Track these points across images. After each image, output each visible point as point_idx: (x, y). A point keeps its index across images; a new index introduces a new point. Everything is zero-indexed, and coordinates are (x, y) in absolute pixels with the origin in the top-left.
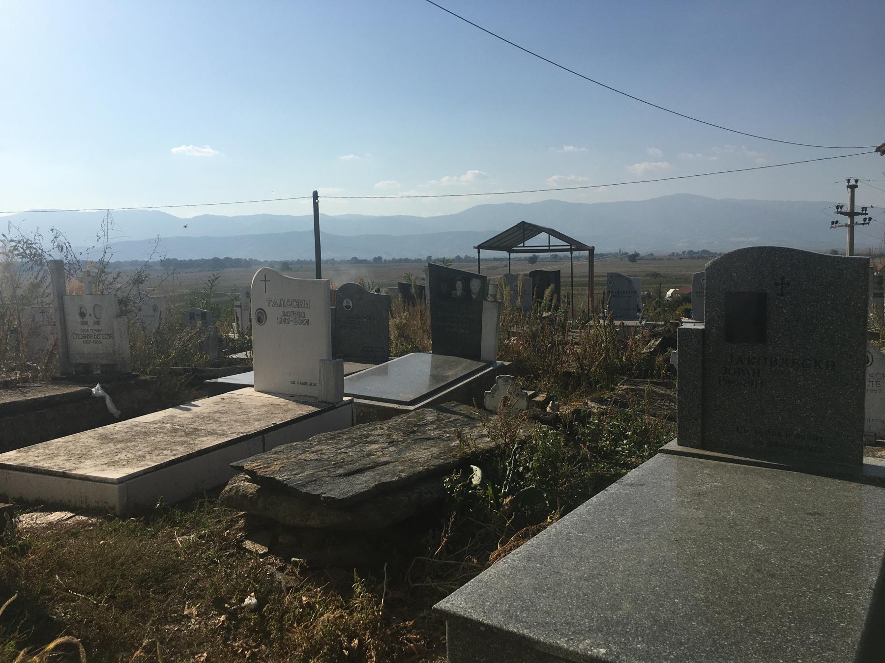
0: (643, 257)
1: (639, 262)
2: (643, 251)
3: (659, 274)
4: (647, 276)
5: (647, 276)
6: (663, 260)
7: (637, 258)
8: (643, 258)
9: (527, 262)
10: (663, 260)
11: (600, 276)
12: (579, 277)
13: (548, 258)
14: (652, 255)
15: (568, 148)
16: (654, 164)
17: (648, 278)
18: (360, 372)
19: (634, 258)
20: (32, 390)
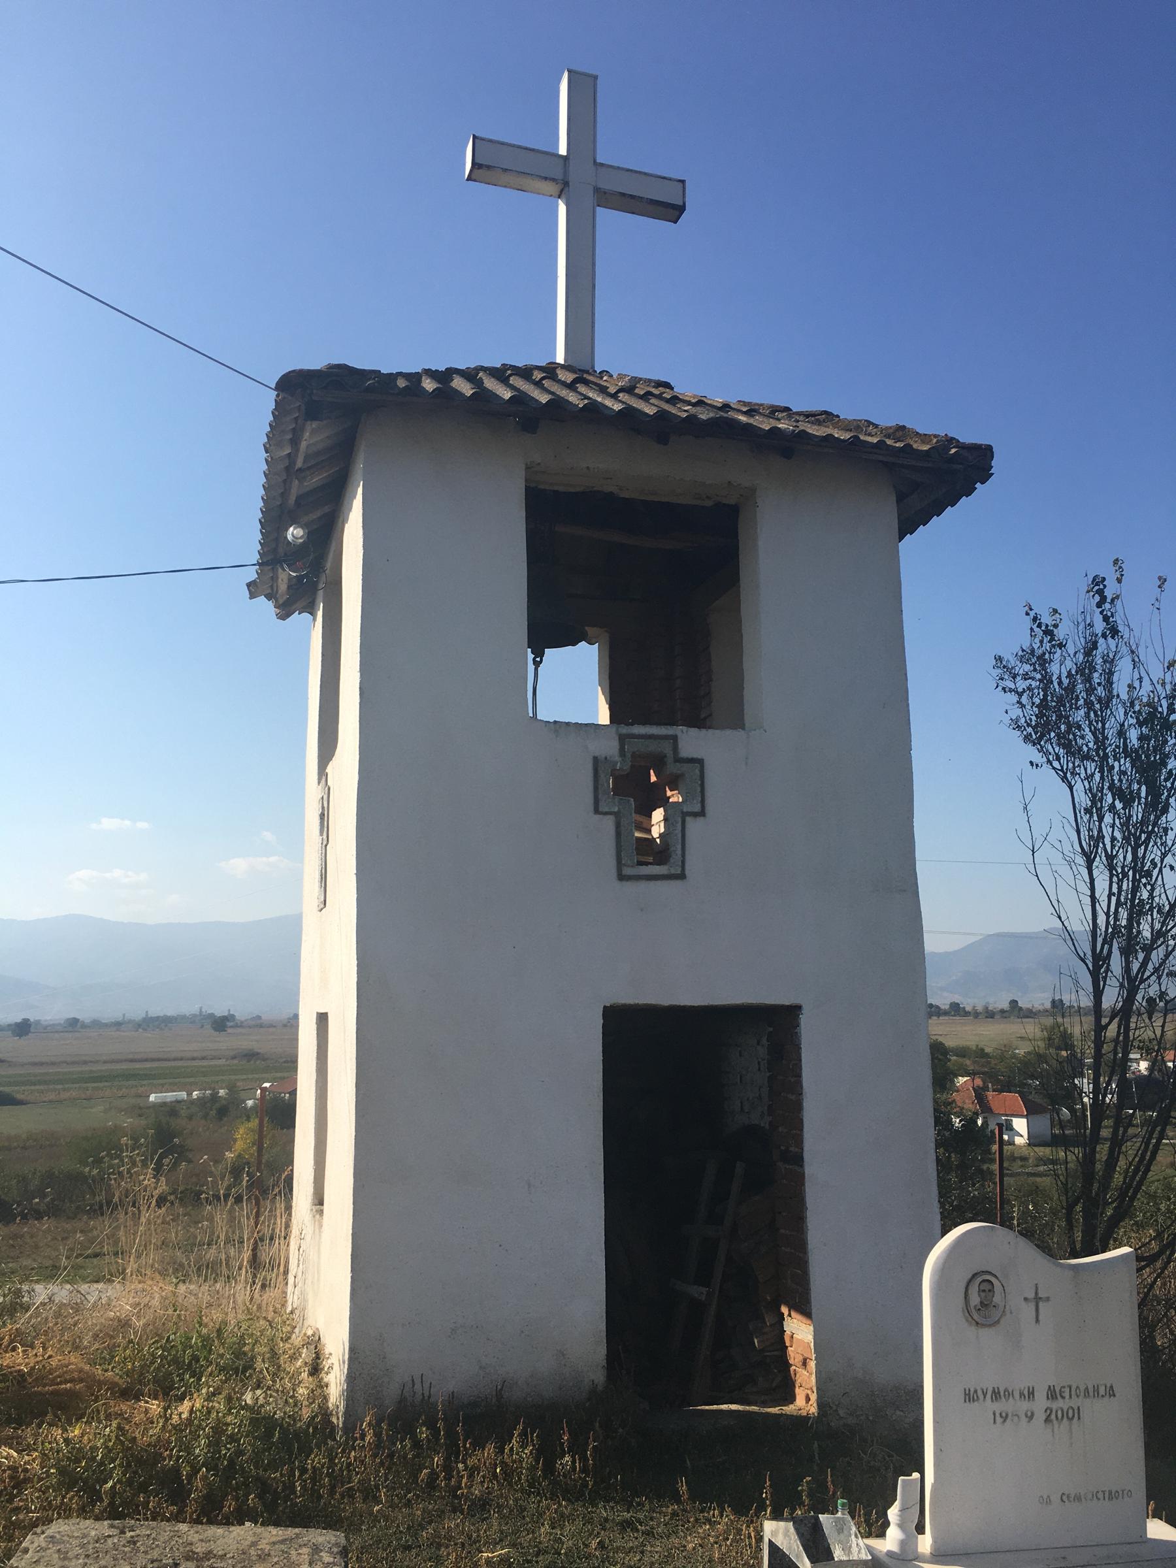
0: (242, 1022)
1: (229, 1030)
2: (242, 1012)
3: (258, 1054)
4: (234, 1058)
5: (234, 1058)
6: (275, 1027)
7: (229, 1024)
8: (240, 1025)
9: (10, 1032)
10: (275, 1027)
11: (146, 1060)
12: (105, 1062)
13: (60, 1024)
14: (259, 1017)
15: (108, 824)
16: (264, 859)
17: (236, 1061)
18: (180, 1063)
19: (221, 1024)
20: (234, 1297)
